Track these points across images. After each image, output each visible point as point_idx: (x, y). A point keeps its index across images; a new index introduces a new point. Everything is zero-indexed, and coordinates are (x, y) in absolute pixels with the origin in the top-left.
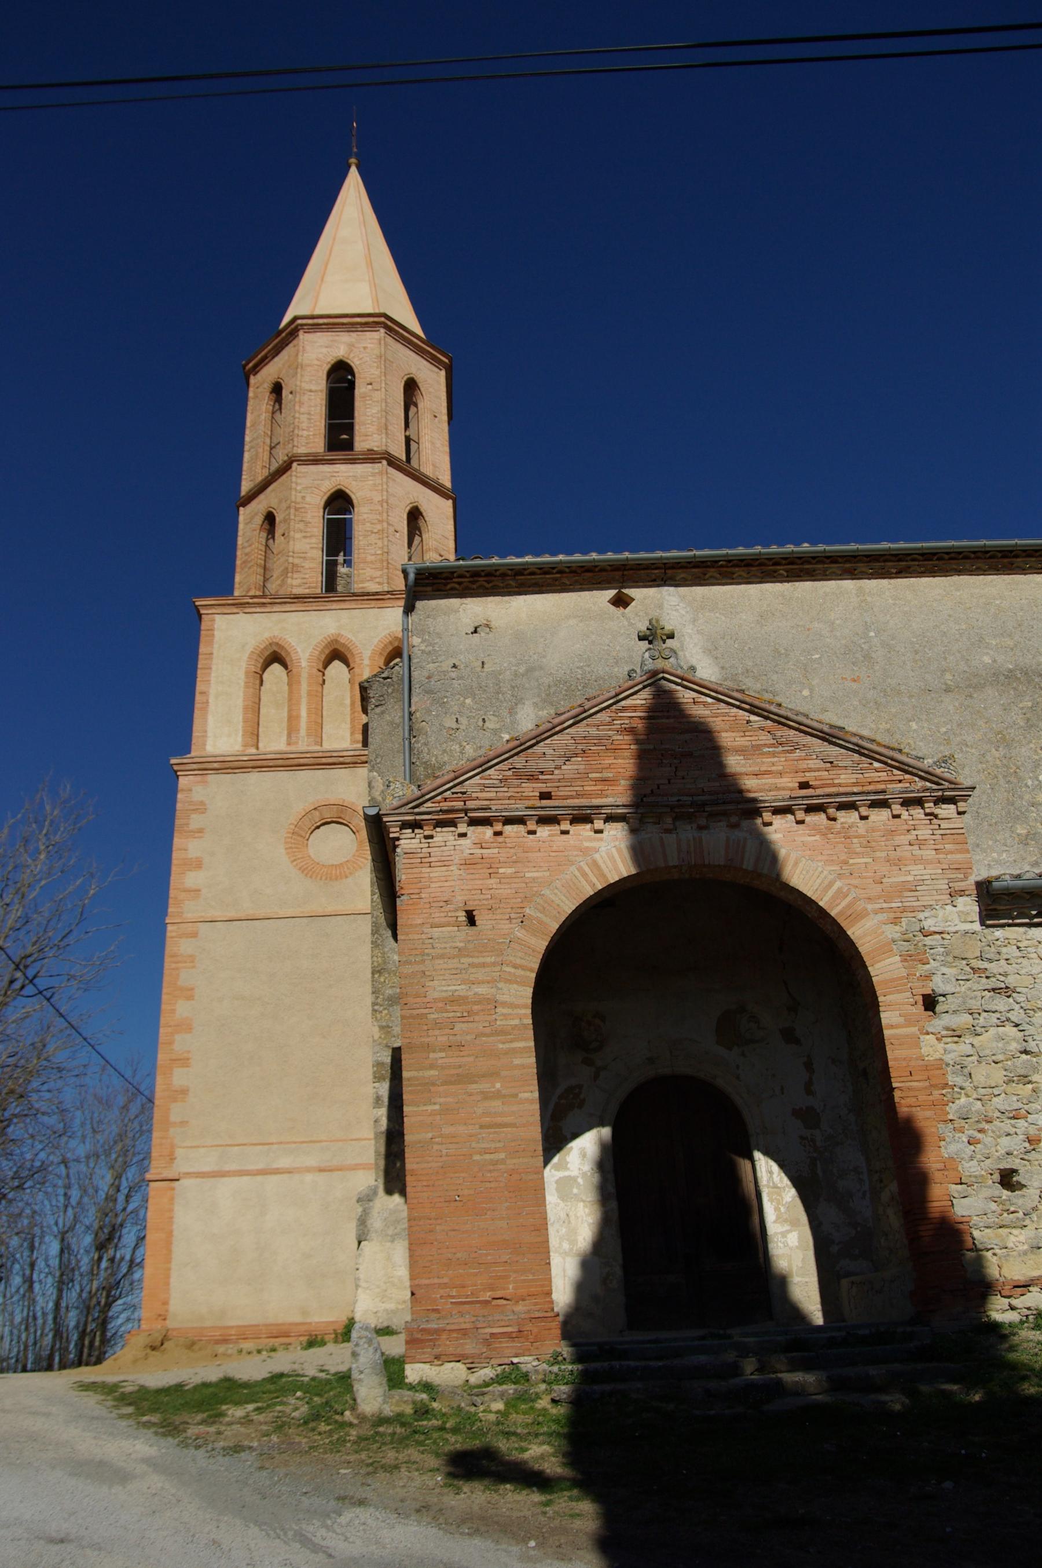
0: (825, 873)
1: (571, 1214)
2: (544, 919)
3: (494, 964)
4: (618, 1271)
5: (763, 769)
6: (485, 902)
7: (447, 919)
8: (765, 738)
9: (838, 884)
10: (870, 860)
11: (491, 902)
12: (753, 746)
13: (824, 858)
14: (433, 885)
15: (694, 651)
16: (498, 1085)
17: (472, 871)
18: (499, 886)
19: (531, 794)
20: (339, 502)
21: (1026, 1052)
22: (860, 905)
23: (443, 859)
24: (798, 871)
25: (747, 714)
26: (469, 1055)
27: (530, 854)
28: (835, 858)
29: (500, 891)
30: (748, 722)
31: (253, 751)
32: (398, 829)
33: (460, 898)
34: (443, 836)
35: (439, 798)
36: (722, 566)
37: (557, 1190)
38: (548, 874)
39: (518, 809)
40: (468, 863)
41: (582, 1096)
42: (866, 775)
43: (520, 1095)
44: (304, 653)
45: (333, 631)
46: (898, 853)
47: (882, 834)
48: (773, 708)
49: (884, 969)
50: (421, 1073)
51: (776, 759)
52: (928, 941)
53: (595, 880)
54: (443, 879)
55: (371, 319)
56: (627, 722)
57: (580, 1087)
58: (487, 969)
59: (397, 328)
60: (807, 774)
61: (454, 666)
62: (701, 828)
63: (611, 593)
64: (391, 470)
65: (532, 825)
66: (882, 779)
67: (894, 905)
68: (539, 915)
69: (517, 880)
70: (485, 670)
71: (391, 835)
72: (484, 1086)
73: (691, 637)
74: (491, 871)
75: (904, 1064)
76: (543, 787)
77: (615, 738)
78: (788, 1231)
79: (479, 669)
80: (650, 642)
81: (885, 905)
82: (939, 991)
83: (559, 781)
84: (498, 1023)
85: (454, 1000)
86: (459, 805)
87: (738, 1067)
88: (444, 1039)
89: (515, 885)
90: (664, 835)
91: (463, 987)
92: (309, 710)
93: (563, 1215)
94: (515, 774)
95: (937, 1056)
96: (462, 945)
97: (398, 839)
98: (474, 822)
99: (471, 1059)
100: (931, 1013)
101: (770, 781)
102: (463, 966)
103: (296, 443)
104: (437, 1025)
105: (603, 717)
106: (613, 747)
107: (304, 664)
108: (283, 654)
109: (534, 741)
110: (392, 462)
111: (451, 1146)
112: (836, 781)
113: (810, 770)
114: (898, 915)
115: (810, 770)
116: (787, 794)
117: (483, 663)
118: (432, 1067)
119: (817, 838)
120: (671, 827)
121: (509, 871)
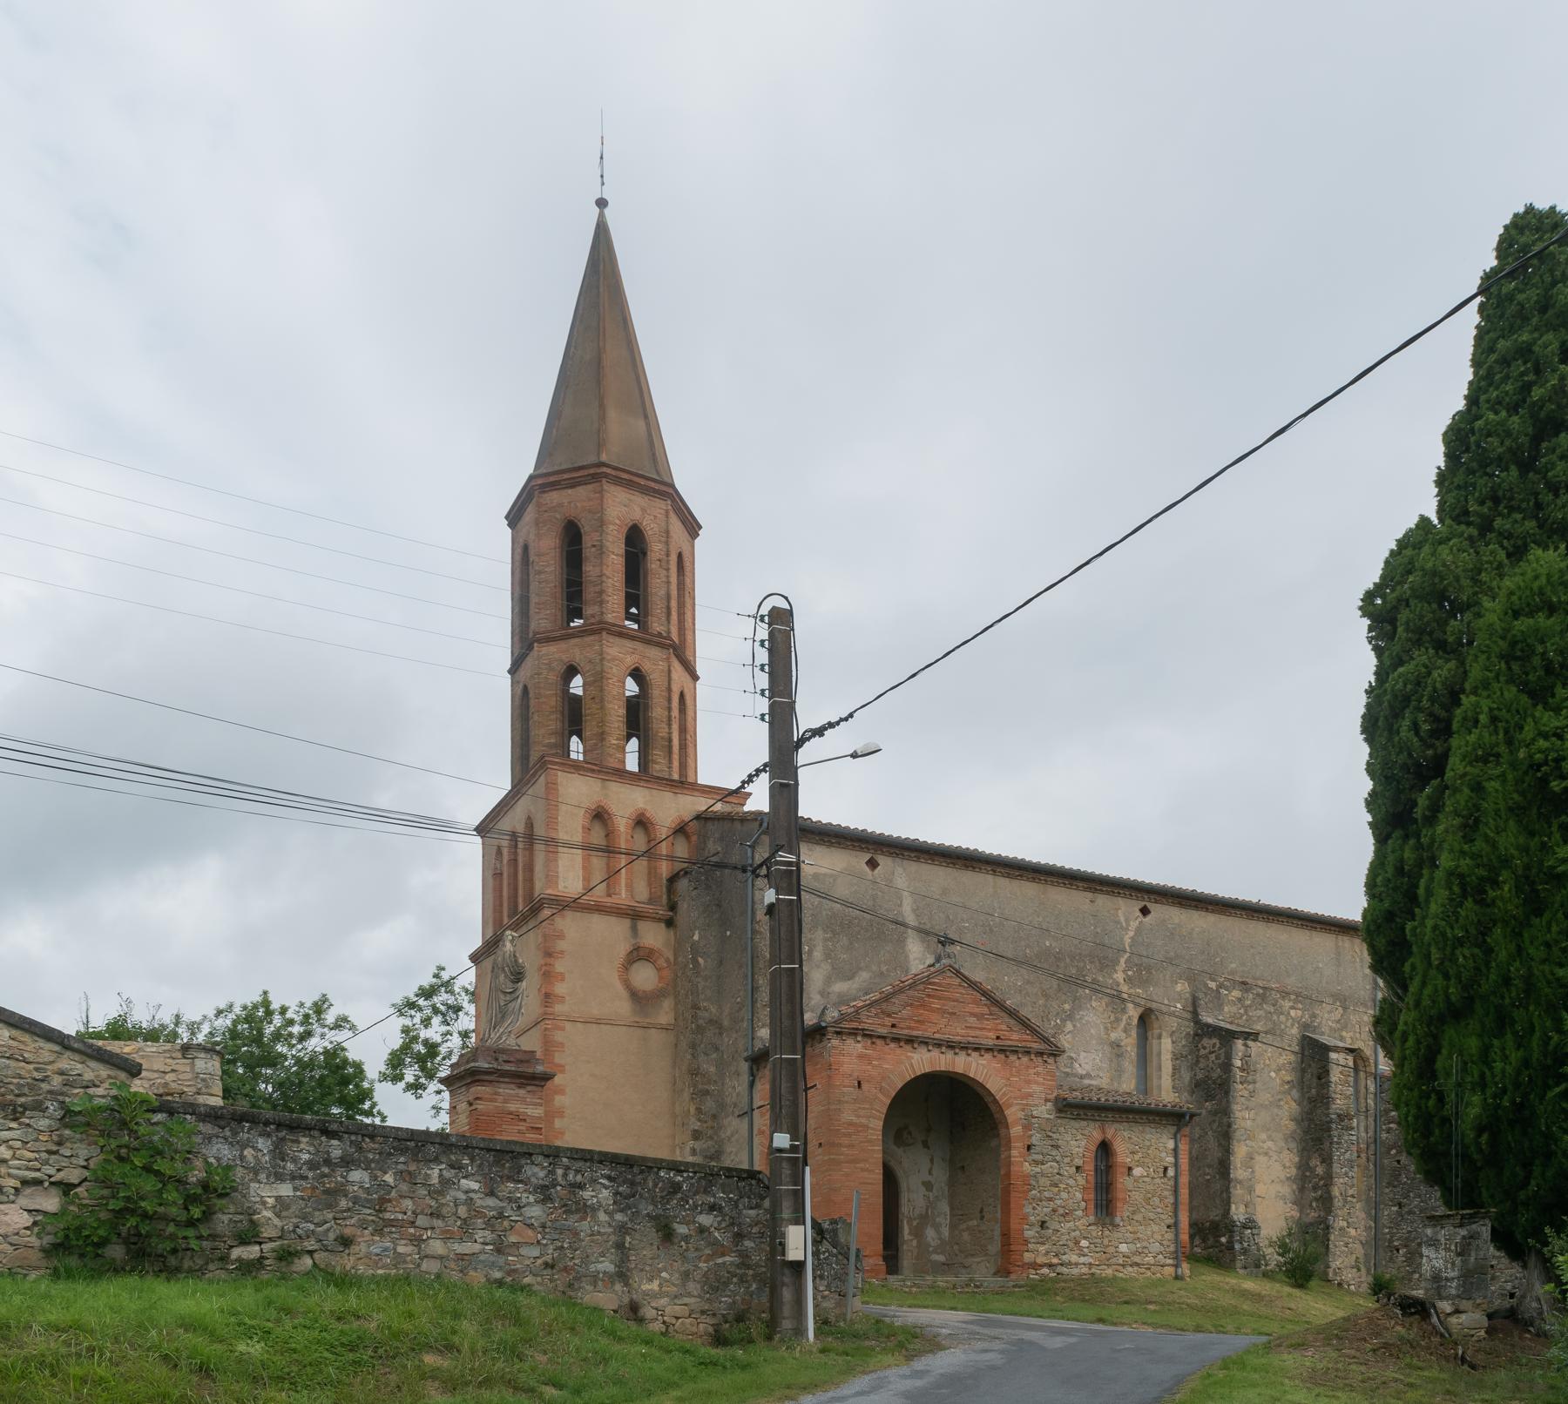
8: (986, 1010)
34: (850, 1041)
39: (883, 1031)
40: (861, 1056)
49: (1016, 1130)
63: (867, 856)
85: (851, 1124)
104: (845, 1135)
107: (622, 829)
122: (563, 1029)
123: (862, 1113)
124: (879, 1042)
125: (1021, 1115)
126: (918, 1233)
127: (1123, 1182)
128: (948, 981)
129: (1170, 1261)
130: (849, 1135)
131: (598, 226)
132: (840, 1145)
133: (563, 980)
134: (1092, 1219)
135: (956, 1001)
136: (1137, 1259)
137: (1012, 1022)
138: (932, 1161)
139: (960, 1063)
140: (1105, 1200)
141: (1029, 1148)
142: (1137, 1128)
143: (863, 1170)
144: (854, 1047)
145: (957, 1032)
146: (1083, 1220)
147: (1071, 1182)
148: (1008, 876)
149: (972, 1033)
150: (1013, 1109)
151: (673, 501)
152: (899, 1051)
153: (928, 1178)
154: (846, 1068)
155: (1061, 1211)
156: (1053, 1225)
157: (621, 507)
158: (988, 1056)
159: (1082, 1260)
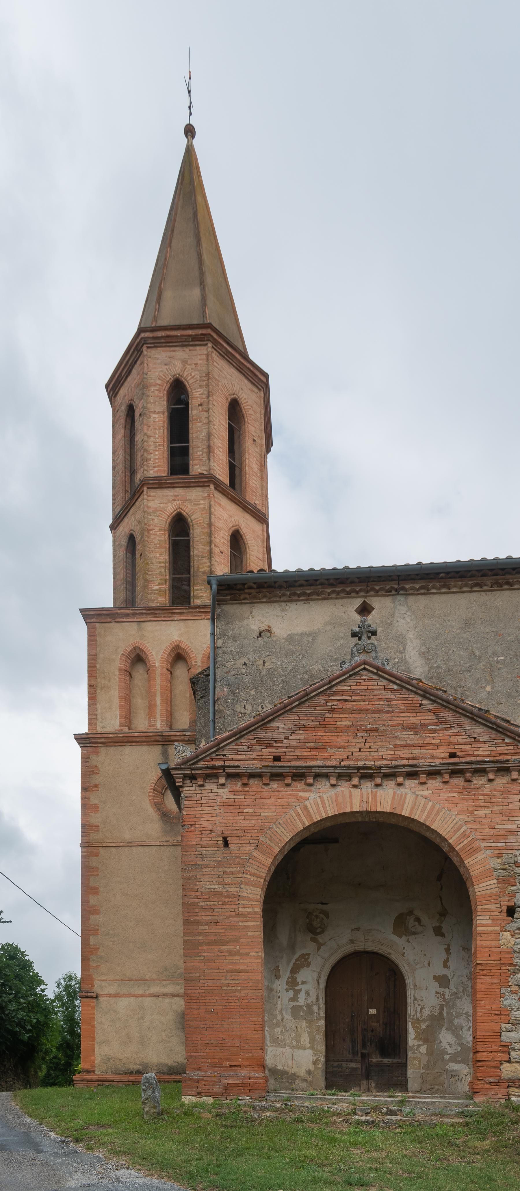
0: (457, 819)
1: (298, 1026)
2: (271, 844)
3: (239, 873)
4: (323, 1059)
5: (426, 742)
6: (235, 832)
7: (211, 842)
8: (430, 718)
9: (464, 828)
11: (239, 831)
12: (421, 724)
13: (458, 809)
14: (203, 819)
15: (412, 654)
16: (238, 947)
17: (227, 811)
18: (244, 821)
19: (268, 757)
20: (180, 526)
22: (476, 844)
23: (210, 801)
24: (438, 818)
25: (420, 698)
26: (221, 929)
27: (264, 800)
28: (465, 809)
29: (245, 825)
30: (421, 705)
31: (126, 730)
32: (181, 780)
33: (220, 828)
34: (211, 787)
35: (208, 758)
36: (442, 578)
37: (291, 1012)
38: (275, 814)
39: (256, 766)
40: (226, 805)
41: (309, 960)
42: (499, 748)
43: (251, 954)
44: (157, 656)
45: (177, 638)
46: (510, 808)
47: (501, 793)
48: (440, 693)
50: (194, 938)
51: (436, 735)
53: (304, 819)
54: (210, 815)
56: (336, 703)
57: (309, 954)
58: (235, 876)
60: (456, 747)
61: (245, 664)
62: (377, 785)
63: (358, 602)
64: (217, 495)
65: (266, 780)
66: (510, 751)
67: (499, 844)
68: (267, 841)
69: (255, 818)
70: (265, 667)
71: (177, 784)
72: (230, 947)
73: (412, 642)
74: (239, 811)
75: (487, 949)
76: (275, 752)
77: (326, 716)
78: (421, 1045)
79: (261, 667)
80: (360, 639)
81: (493, 844)
83: (287, 748)
84: (240, 909)
85: (214, 894)
86: (219, 763)
87: (404, 948)
88: (208, 918)
89: (253, 821)
90: (352, 790)
91: (220, 886)
92: (162, 700)
93: (294, 1027)
94: (258, 742)
95: (509, 945)
96: (220, 859)
97: (182, 787)
98: (229, 776)
99: (223, 931)
100: (511, 918)
102: (220, 873)
103: (145, 468)
104: (204, 909)
105: (321, 700)
106: (324, 723)
107: (157, 664)
108: (144, 656)
109: (271, 717)
110: (218, 486)
111: (210, 981)
112: (476, 753)
113: (459, 744)
114: (502, 851)
115: (459, 744)
116: (437, 761)
117: (264, 662)
118: (200, 934)
119: (455, 794)
120: (357, 783)
121: (251, 811)
122: (97, 855)
123: (229, 878)
124: (253, 782)
126: (428, 1037)
128: (364, 685)
130: (212, 909)
132: (198, 923)
133: (97, 811)
135: (381, 711)
137: (478, 729)
138: (448, 951)
139: (385, 798)
144: (217, 793)
145: (383, 753)
149: (405, 753)
150: (480, 856)
151: (215, 343)
152: (284, 791)
153: (441, 971)
154: (204, 823)
158: (434, 783)
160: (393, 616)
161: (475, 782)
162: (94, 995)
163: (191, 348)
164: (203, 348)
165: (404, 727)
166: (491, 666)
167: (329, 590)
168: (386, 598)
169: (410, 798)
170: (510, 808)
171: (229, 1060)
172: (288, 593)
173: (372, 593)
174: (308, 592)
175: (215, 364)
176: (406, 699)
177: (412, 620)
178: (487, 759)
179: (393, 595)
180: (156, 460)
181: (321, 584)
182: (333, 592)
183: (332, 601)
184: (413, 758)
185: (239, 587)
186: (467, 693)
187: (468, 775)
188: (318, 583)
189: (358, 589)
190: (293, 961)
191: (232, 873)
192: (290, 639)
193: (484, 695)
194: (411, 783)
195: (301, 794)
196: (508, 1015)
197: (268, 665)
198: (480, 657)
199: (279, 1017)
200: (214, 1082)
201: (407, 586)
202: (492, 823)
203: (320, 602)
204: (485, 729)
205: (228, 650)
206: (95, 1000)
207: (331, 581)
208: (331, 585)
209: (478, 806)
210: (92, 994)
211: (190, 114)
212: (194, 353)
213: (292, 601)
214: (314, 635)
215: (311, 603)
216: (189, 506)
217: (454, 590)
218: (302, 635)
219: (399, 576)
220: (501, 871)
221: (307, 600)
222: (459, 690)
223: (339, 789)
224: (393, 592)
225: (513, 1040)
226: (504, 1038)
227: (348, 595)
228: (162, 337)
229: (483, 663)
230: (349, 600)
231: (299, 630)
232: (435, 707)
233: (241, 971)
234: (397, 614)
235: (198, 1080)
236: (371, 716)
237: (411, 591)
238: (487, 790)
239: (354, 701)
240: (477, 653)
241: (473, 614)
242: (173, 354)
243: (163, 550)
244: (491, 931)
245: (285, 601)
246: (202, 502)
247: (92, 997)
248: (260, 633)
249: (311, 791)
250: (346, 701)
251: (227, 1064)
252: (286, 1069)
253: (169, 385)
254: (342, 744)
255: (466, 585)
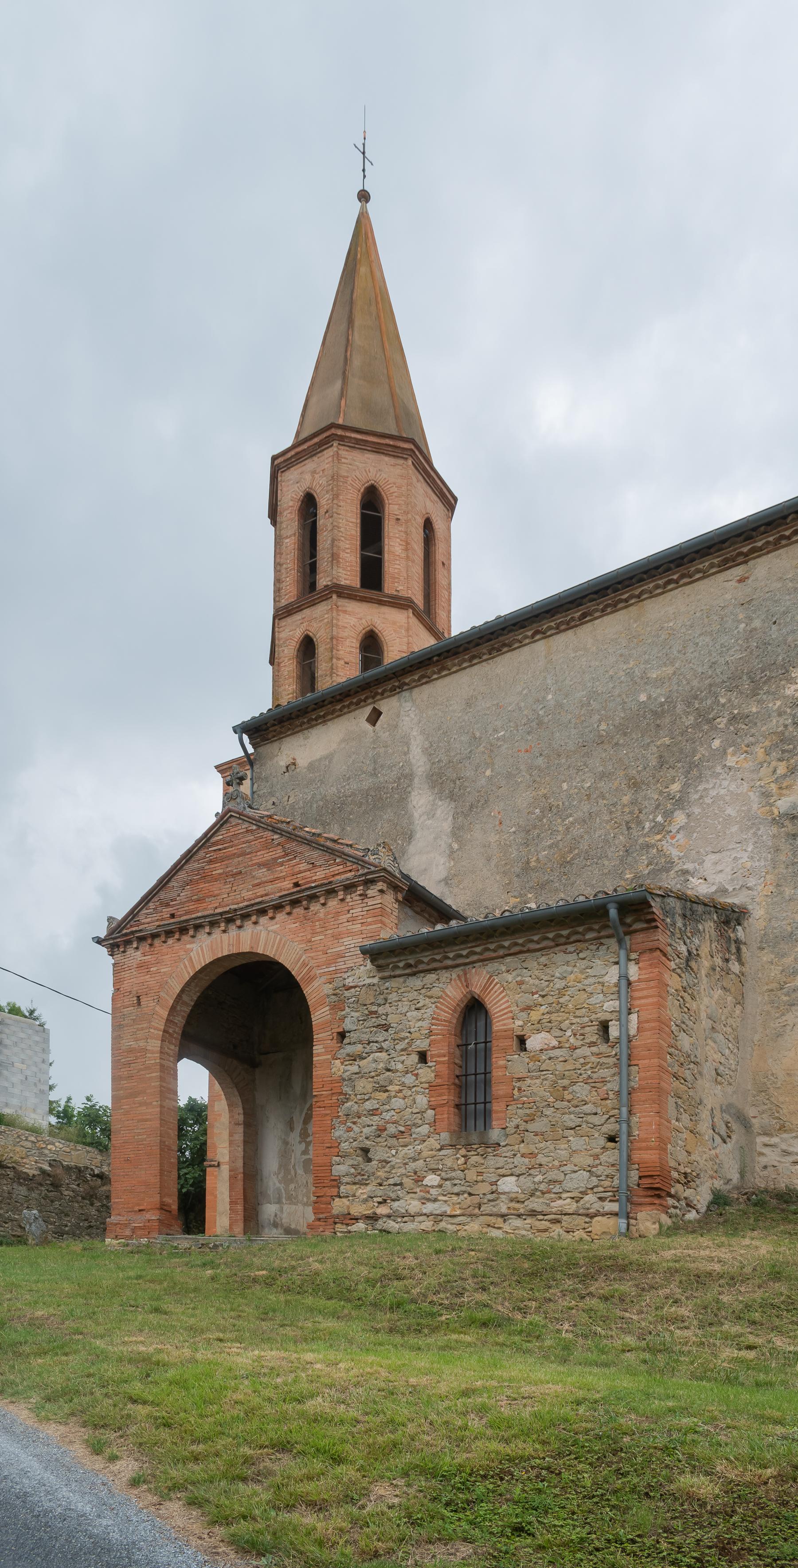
3: (146, 1028)
10: (323, 937)
21: (389, 1070)
36: (438, 661)
40: (140, 966)
49: (319, 1015)
52: (347, 994)
55: (316, 440)
59: (348, 434)
61: (274, 804)
62: (240, 927)
63: (368, 710)
64: (342, 602)
67: (331, 969)
76: (170, 910)
81: (326, 970)
82: (347, 1029)
83: (179, 904)
95: (340, 1073)
101: (279, 885)
112: (314, 878)
121: (155, 969)
125: (328, 989)
127: (506, 1065)
129: (614, 1207)
131: (359, 222)
134: (445, 1136)
135: (243, 854)
136: (536, 1204)
137: (316, 854)
140: (471, 1099)
141: (342, 1035)
142: (533, 962)
143: (141, 1104)
145: (244, 894)
146: (430, 1141)
147: (409, 1079)
148: (569, 626)
150: (316, 984)
151: (341, 438)
152: (177, 946)
155: (392, 1129)
156: (378, 1153)
157: (364, 468)
158: (281, 916)
159: (429, 1207)
160: (398, 716)
161: (312, 908)
162: (216, 1163)
163: (319, 455)
164: (330, 449)
165: (260, 865)
166: (491, 745)
167: (338, 707)
168: (393, 698)
169: (263, 935)
170: (339, 930)
171: (139, 1205)
172: (305, 720)
173: (378, 697)
174: (322, 714)
175: (343, 460)
176: (262, 837)
177: (416, 715)
178: (313, 885)
179: (399, 693)
180: (343, 565)
181: (331, 703)
182: (344, 707)
183: (346, 716)
184: (266, 895)
185: (264, 727)
186: (466, 784)
187: (305, 903)
188: (326, 702)
189: (363, 697)
190: (305, 1111)
191: (142, 1029)
192: (311, 767)
193: (483, 781)
194: (263, 920)
195: (188, 946)
196: (337, 1147)
197: (292, 800)
198: (480, 738)
199: (293, 1172)
200: (126, 1225)
201: (407, 681)
202: (326, 948)
203: (336, 720)
204: (321, 852)
205: (261, 793)
206: (217, 1169)
207: (338, 697)
208: (340, 701)
209: (314, 933)
210: (213, 1163)
211: (364, 177)
212: (322, 459)
213: (312, 727)
214: (329, 757)
215: (329, 723)
216: (315, 625)
217: (454, 669)
218: (320, 760)
219: (394, 674)
220: (333, 997)
221: (325, 721)
222: (458, 782)
223: (214, 936)
224: (398, 690)
225: (341, 1174)
226: (334, 1173)
227: (358, 705)
228: (292, 457)
229: (484, 744)
230: (360, 710)
231: (318, 756)
232: (283, 839)
233: (146, 1120)
234: (402, 713)
235: (117, 1224)
236: (236, 860)
237: (414, 684)
238: (321, 915)
239: (225, 848)
240: (478, 735)
241: (474, 690)
242: (304, 468)
243: (291, 680)
244: (325, 1060)
245: (307, 729)
246: (326, 616)
247: (214, 1166)
248: (287, 767)
249: (194, 942)
250: (220, 850)
251: (137, 1208)
252: (298, 1228)
253: (300, 503)
254: (216, 892)
255: (465, 661)
